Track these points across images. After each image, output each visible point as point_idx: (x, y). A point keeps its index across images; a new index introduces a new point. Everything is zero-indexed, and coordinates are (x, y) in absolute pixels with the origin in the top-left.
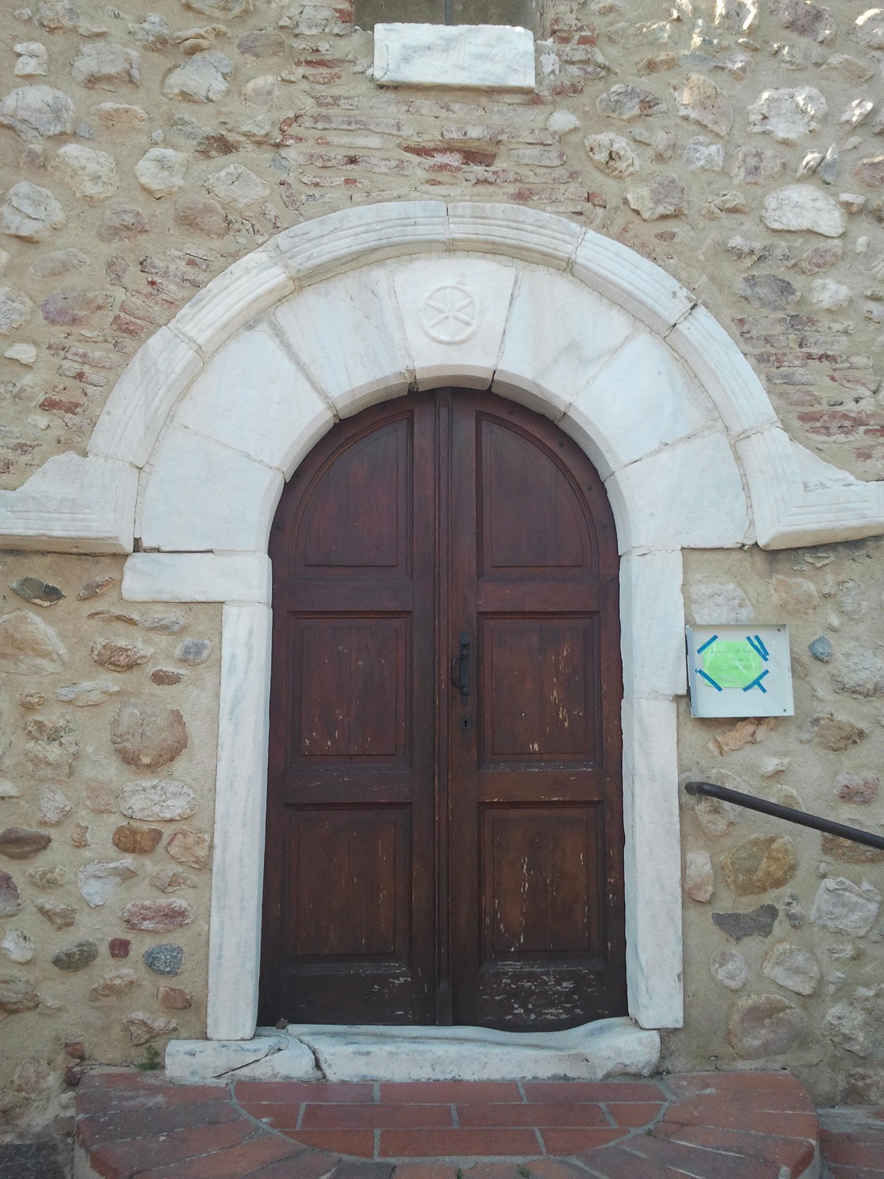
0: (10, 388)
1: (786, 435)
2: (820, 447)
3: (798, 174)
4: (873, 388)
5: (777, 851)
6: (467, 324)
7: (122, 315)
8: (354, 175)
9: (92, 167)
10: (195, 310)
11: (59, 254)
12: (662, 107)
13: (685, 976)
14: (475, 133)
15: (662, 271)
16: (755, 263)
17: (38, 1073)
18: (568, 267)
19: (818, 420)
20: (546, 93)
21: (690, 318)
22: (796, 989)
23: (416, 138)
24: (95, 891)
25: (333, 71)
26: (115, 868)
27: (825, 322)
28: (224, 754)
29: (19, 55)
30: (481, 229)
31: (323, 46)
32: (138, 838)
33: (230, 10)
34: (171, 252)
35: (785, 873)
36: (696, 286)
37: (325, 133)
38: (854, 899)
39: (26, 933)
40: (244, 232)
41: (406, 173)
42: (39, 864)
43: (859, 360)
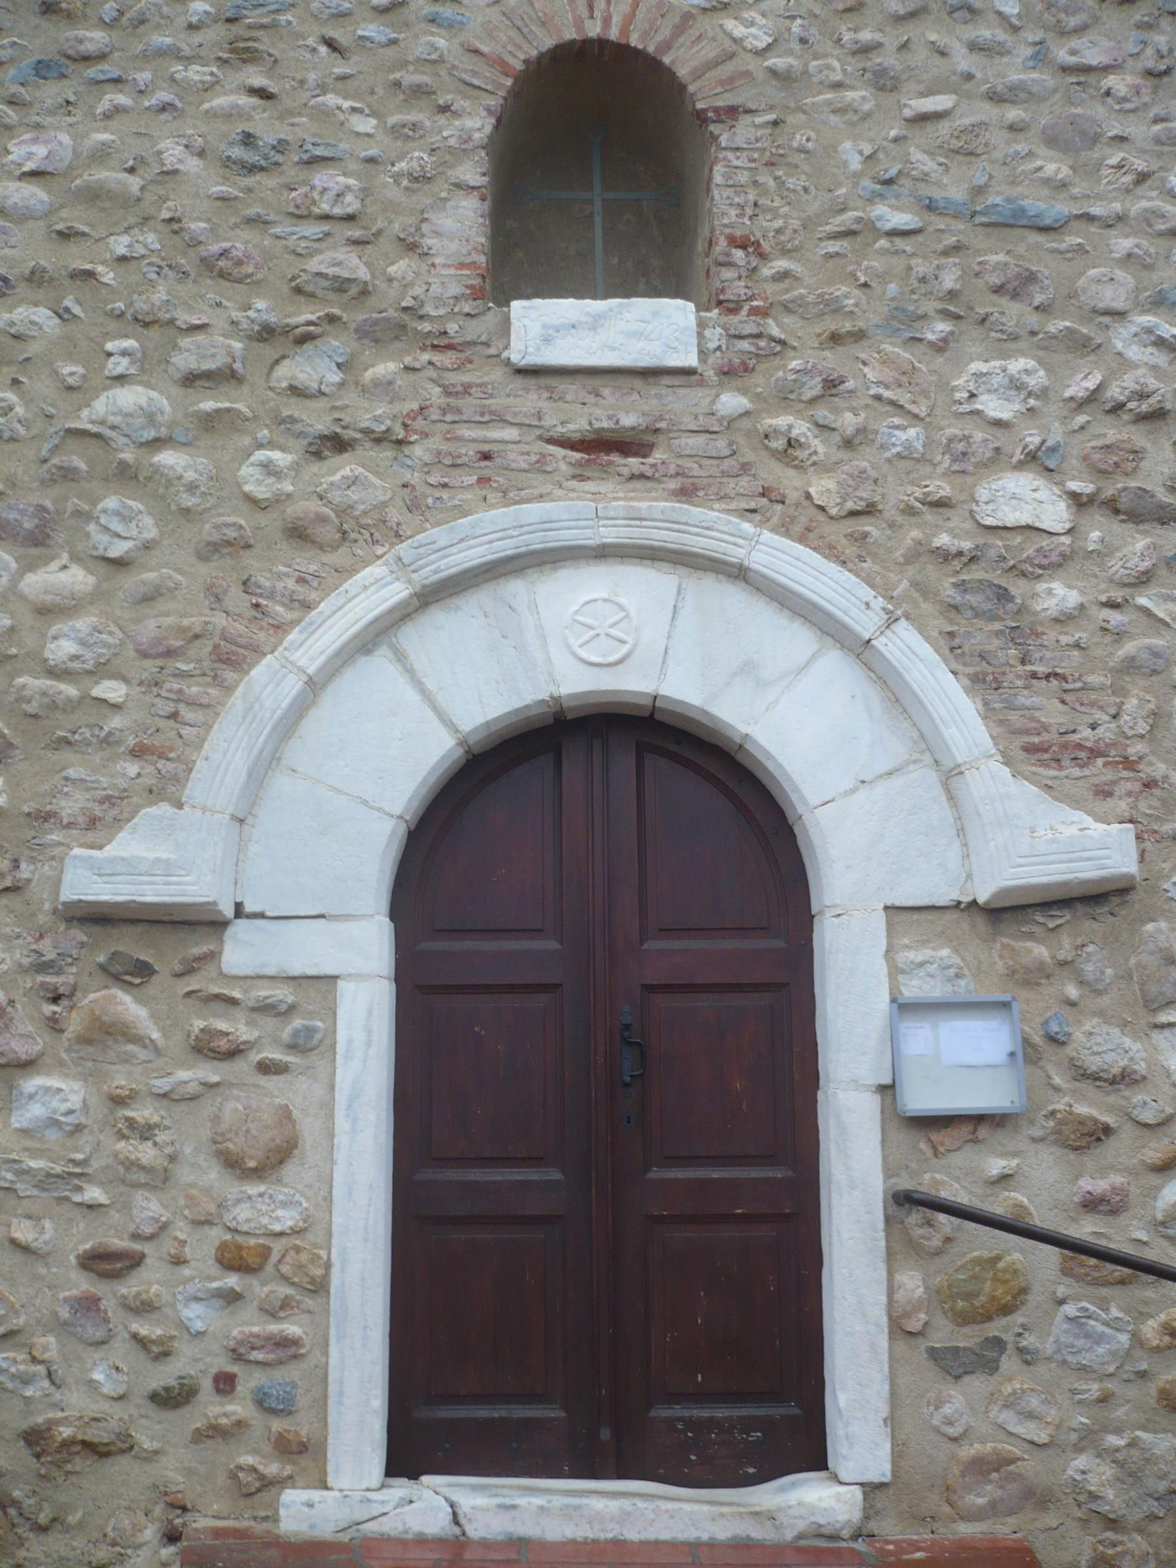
0: (97, 732)
1: (1007, 770)
2: (1050, 783)
3: (1014, 460)
4: (1113, 711)
5: (1004, 1271)
6: (623, 642)
7: (222, 643)
8: (487, 473)
9: (190, 475)
10: (305, 634)
11: (151, 576)
12: (850, 384)
13: (892, 1421)
14: (628, 421)
15: (853, 578)
16: (965, 564)
17: (134, 1525)
18: (739, 574)
19: (1046, 751)
20: (712, 372)
21: (888, 632)
22: (1028, 1437)
23: (560, 429)
24: (196, 1315)
25: (463, 355)
26: (218, 1289)
27: (1051, 635)
28: (340, 1155)
29: (110, 355)
30: (636, 532)
31: (452, 328)
32: (244, 1254)
33: (345, 291)
34: (278, 569)
35: (1014, 1297)
36: (895, 594)
37: (455, 426)
38: (1100, 1328)
39: (117, 1363)
40: (361, 543)
41: (549, 469)
42: (129, 1288)
43: (1094, 679)
